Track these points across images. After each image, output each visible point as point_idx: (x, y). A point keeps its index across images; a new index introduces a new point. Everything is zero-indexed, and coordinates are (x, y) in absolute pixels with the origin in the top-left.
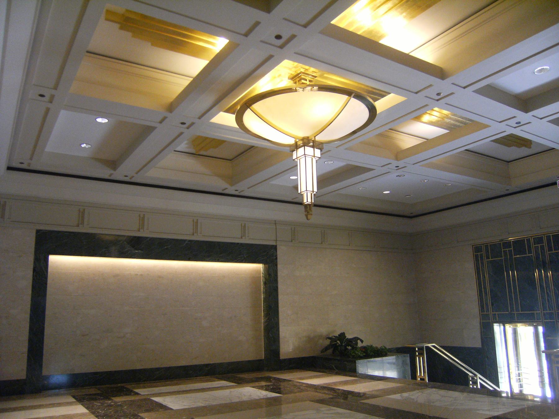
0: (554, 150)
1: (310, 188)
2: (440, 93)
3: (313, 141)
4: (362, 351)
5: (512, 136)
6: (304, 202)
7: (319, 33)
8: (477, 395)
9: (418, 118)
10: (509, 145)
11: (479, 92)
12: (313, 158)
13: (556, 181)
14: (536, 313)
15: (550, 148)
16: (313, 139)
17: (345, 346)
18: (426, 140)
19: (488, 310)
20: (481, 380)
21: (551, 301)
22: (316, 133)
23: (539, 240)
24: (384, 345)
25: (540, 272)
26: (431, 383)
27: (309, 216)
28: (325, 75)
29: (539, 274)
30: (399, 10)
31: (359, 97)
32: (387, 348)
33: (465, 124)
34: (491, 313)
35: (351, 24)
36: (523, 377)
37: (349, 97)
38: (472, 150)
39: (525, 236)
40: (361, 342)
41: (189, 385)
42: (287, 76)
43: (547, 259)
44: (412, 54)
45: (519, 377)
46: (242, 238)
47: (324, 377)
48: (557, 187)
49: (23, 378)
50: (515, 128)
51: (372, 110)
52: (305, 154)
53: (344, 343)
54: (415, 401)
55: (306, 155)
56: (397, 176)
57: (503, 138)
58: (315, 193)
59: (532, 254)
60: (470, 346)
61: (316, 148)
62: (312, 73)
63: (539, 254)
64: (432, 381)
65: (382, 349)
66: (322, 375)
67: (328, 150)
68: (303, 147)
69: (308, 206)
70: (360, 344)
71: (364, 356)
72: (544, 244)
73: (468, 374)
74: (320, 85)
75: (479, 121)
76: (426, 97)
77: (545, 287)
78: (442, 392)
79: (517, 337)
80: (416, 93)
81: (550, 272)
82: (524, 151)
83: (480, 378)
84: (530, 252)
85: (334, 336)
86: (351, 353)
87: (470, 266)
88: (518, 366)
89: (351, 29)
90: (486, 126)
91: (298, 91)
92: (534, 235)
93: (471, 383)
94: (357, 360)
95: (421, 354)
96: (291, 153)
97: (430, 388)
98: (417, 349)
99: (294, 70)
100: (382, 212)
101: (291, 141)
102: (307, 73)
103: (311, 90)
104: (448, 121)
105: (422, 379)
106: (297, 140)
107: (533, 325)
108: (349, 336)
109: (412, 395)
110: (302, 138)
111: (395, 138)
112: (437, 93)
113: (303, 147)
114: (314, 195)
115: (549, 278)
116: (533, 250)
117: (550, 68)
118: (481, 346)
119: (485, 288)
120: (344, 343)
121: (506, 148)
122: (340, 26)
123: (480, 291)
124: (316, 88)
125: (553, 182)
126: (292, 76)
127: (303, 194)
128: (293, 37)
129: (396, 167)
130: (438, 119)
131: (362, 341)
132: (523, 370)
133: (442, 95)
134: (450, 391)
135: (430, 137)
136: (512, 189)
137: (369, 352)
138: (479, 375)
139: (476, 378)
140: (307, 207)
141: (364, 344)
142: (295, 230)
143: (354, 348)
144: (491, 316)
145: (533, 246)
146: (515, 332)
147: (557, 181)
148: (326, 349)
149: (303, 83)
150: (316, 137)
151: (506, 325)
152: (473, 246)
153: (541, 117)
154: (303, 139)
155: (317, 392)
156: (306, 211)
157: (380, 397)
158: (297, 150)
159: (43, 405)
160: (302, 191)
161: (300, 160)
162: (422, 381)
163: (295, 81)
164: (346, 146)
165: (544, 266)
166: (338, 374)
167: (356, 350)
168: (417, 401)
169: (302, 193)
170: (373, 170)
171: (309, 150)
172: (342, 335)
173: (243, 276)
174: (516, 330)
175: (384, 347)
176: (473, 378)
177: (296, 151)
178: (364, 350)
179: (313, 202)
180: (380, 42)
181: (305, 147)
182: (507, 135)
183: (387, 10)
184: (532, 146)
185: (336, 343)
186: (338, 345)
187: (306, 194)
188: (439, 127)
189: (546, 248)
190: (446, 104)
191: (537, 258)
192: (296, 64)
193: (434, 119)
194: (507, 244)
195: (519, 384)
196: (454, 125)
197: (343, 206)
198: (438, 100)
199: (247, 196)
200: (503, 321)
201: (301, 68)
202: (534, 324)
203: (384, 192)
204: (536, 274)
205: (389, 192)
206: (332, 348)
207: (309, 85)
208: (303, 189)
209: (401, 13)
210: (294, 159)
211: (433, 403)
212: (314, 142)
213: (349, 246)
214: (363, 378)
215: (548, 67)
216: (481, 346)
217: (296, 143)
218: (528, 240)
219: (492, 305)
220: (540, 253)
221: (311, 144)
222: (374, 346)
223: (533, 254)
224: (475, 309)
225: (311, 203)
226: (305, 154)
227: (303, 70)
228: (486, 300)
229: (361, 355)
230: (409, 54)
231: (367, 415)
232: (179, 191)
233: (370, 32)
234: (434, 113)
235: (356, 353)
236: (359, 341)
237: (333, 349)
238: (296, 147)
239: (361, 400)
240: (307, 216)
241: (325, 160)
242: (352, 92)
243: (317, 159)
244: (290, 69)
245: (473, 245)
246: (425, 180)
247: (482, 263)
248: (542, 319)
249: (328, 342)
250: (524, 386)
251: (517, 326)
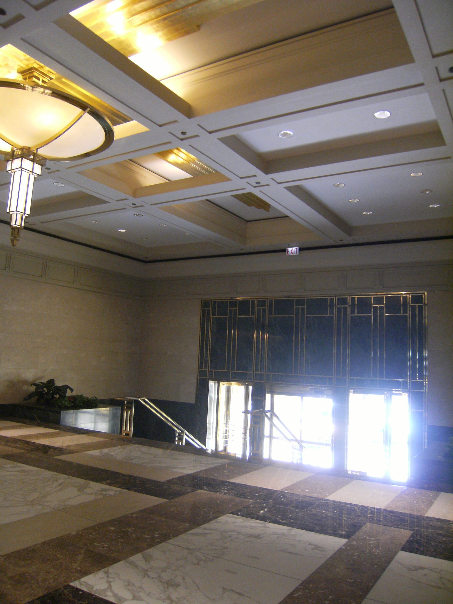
0: (287, 218)
1: (21, 209)
2: (185, 132)
3: (34, 153)
4: (70, 401)
5: (250, 194)
6: (12, 224)
7: (217, 139)
8: (178, 452)
9: (163, 155)
10: (249, 205)
11: (223, 140)
12: (31, 174)
13: (285, 249)
14: (249, 373)
15: (284, 216)
16: (34, 152)
17: (53, 394)
18: (169, 181)
19: (206, 367)
20: (188, 437)
21: (264, 363)
22: (40, 144)
23: (262, 303)
24: (96, 396)
25: (258, 333)
26: (136, 438)
27: (15, 241)
28: (64, 80)
29: (258, 336)
30: (155, 26)
31: (95, 114)
32: (98, 399)
33: (210, 172)
34: (208, 369)
35: (100, 25)
36: (229, 434)
37: (83, 112)
38: (212, 201)
39: (251, 298)
40: (71, 391)
42: (16, 68)
43: (267, 322)
44: (162, 82)
45: (226, 434)
46: (5, 269)
47: (22, 428)
48: (286, 254)
49: (223, 382)
50: (255, 187)
51: (109, 133)
52: (21, 167)
53: (52, 390)
54: (114, 457)
55: (22, 169)
56: (134, 215)
57: (243, 194)
58: (26, 215)
59: (254, 316)
60: (183, 401)
61: (37, 163)
62: (48, 73)
63: (260, 316)
64: (136, 437)
65: (93, 400)
66: (20, 425)
67: (56, 170)
68: (21, 159)
69: (16, 230)
70: (69, 393)
71: (71, 406)
72: (266, 308)
73: (175, 431)
74: (56, 90)
75: (226, 175)
76: (170, 133)
77: (260, 349)
78: (144, 449)
79: (230, 395)
80: (160, 126)
81: (267, 335)
82: (261, 213)
83: (186, 434)
84: (253, 313)
85: (41, 383)
86: (57, 403)
87: (196, 321)
88: (227, 424)
89: (98, 33)
90: (227, 179)
91: (27, 89)
92: (259, 298)
93: (177, 439)
94: (63, 410)
95: (129, 408)
96: (6, 162)
97: (134, 443)
98: (126, 403)
99: (26, 62)
100: (84, 242)
101: (7, 148)
102: (41, 70)
103: (43, 93)
104: (194, 165)
105: (127, 434)
106: (15, 149)
107: (245, 385)
108: (58, 383)
109: (113, 451)
110: (20, 148)
111: (137, 172)
112: (181, 132)
113: (21, 159)
114: (26, 217)
115: (265, 341)
116: (256, 313)
117: (293, 134)
118: (194, 403)
119: (207, 344)
120: (52, 390)
121: (246, 206)
122: (96, 33)
123: (202, 348)
124: (47, 91)
125: (282, 248)
126: (22, 70)
127: (12, 215)
128: (20, 18)
129: (133, 204)
130: (183, 162)
131: (72, 390)
132: (231, 427)
133: (187, 135)
134: (152, 448)
135: (173, 178)
136: (246, 250)
137: (78, 403)
138: (185, 431)
139: (182, 434)
140: (16, 230)
141: (74, 393)
142: (11, 256)
143: (63, 396)
144: (208, 374)
145: (256, 309)
146: (228, 390)
147: (287, 249)
148: (31, 396)
149: (34, 82)
150: (38, 150)
151: (221, 382)
152: (202, 300)
153: (279, 182)
154: (23, 149)
155: (8, 445)
156: (12, 234)
157: (77, 452)
158: (12, 161)
160: (10, 211)
161: (14, 173)
162: (127, 437)
163: (25, 77)
164: (79, 169)
165: (263, 328)
166: (39, 425)
167: (64, 399)
168: (115, 458)
169: (11, 213)
170: (109, 202)
171: (27, 164)
172: (51, 382)
174: (230, 388)
175: (96, 397)
176: (179, 434)
177: (11, 161)
178: (72, 400)
179: (23, 225)
180: (129, 58)
181: (23, 159)
182: (248, 193)
184: (270, 209)
185: (42, 390)
186: (44, 392)
187: (15, 215)
188: (184, 171)
189: (267, 312)
190: (190, 145)
191: (258, 320)
192: (28, 56)
193: (180, 160)
194: (233, 303)
195: (224, 441)
196: (200, 172)
197: (71, 238)
198: (182, 140)
200: (219, 379)
201: (34, 63)
202: (246, 384)
203: (119, 230)
204: (255, 336)
205: (125, 231)
206: (37, 395)
207: (41, 86)
208: (13, 208)
209: (157, 31)
210: (7, 170)
211: (132, 460)
212: (35, 155)
213: (74, 283)
214: (65, 431)
215: (292, 133)
216: (194, 403)
217: (13, 151)
218: (253, 302)
219: (211, 361)
220: (261, 316)
221: (32, 157)
222: (85, 396)
223: (255, 316)
224: (194, 364)
225: (19, 227)
226: (21, 167)
227: (36, 66)
228: (206, 357)
229: (69, 405)
230: (160, 82)
231: (56, 473)
233: (121, 42)
234: (181, 154)
235: (63, 403)
236: (68, 390)
237: (37, 397)
238: (12, 156)
239: (55, 456)
240: (12, 241)
241: (56, 181)
242: (87, 107)
243: (35, 176)
244: (21, 61)
245: (203, 299)
246: (164, 225)
247: (208, 319)
248: (253, 379)
249: (33, 388)
250: (229, 442)
251: (231, 384)
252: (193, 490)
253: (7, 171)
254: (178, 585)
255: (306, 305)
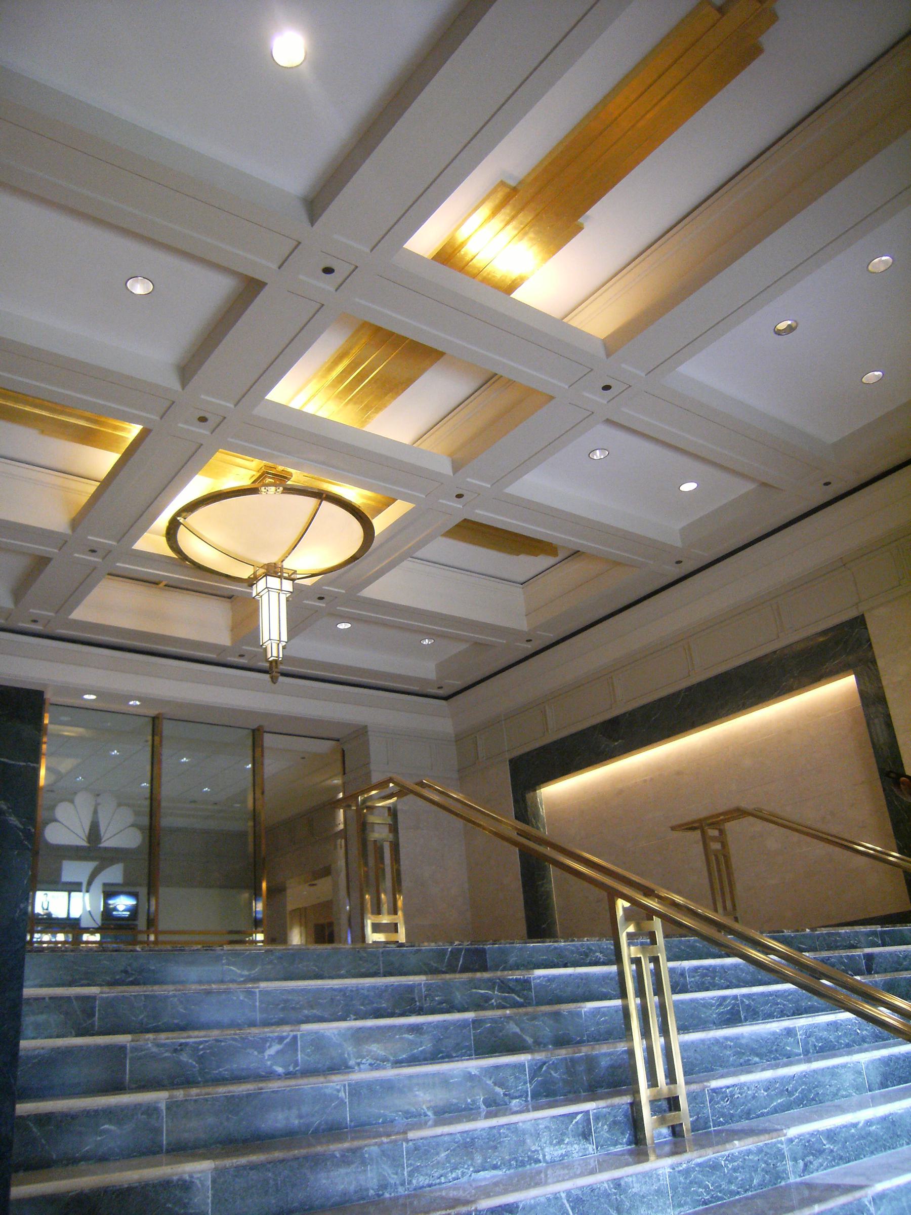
1: (275, 636)
41: (817, 1018)
114: (284, 648)
159: (302, 1073)
171: (273, 582)
173: (830, 714)
179: (281, 656)
183: (476, 258)
187: (270, 645)
199: (838, 501)
232: (883, 480)
252: (425, 964)
253: (254, 598)
254: (199, 1083)
255: (290, 470)
